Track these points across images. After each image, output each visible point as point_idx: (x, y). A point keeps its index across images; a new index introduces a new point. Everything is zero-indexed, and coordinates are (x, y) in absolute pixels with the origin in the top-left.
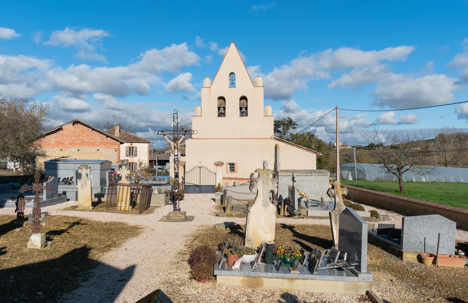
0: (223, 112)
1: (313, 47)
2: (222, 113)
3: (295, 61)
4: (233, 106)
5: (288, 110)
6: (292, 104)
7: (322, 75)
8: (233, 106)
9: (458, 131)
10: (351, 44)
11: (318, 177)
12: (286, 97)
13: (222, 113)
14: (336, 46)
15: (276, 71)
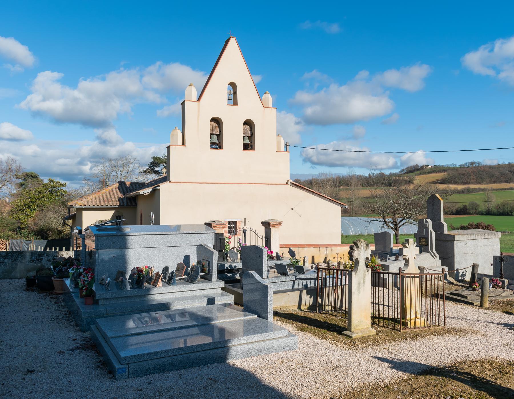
0: (216, 141)
1: (140, 58)
2: (217, 143)
3: (113, 75)
4: (233, 135)
5: (104, 142)
6: (111, 134)
7: (152, 97)
8: (233, 135)
9: (328, 176)
10: (185, 62)
11: (490, 240)
12: (101, 124)
13: (217, 143)
14: (168, 60)
15: (85, 84)
